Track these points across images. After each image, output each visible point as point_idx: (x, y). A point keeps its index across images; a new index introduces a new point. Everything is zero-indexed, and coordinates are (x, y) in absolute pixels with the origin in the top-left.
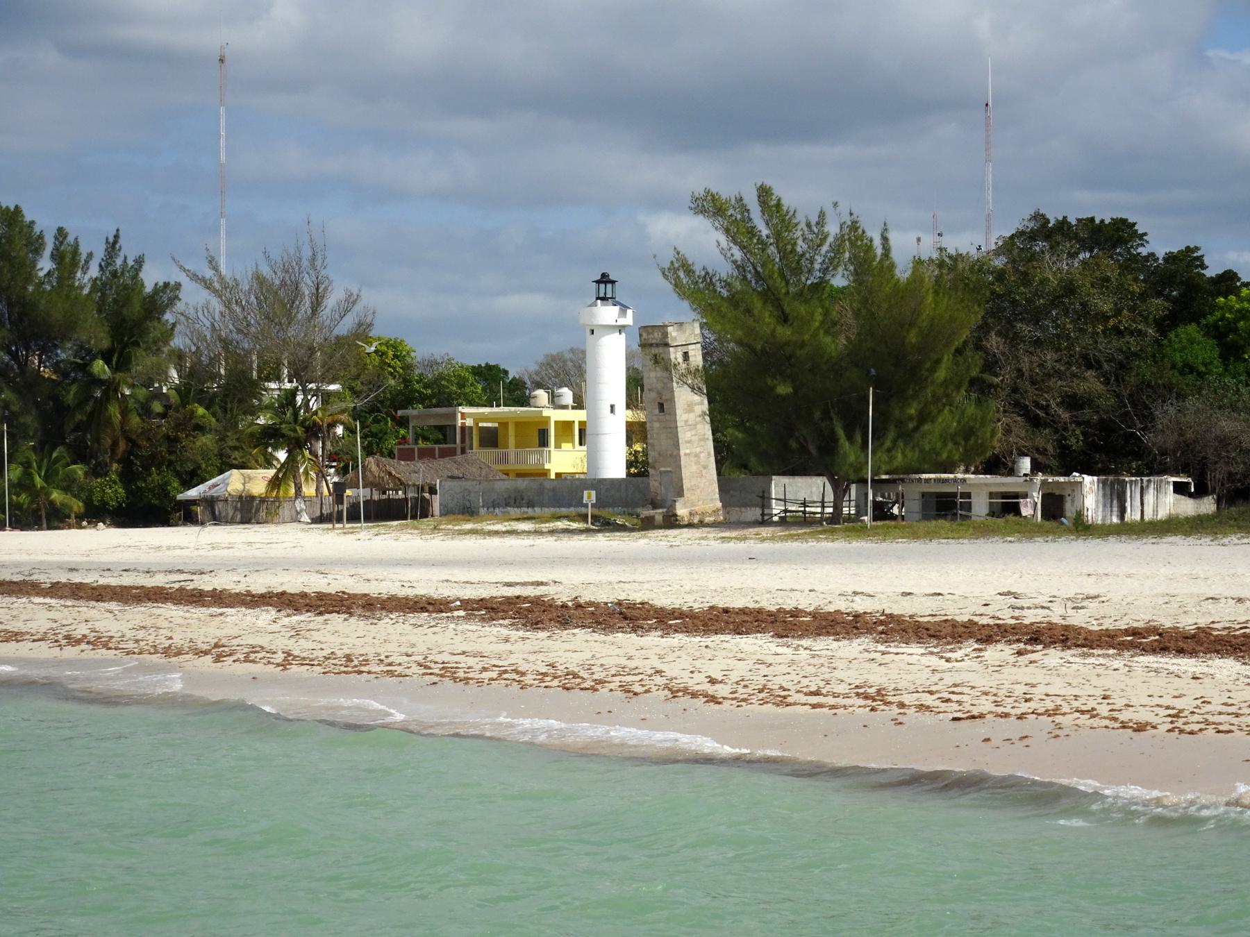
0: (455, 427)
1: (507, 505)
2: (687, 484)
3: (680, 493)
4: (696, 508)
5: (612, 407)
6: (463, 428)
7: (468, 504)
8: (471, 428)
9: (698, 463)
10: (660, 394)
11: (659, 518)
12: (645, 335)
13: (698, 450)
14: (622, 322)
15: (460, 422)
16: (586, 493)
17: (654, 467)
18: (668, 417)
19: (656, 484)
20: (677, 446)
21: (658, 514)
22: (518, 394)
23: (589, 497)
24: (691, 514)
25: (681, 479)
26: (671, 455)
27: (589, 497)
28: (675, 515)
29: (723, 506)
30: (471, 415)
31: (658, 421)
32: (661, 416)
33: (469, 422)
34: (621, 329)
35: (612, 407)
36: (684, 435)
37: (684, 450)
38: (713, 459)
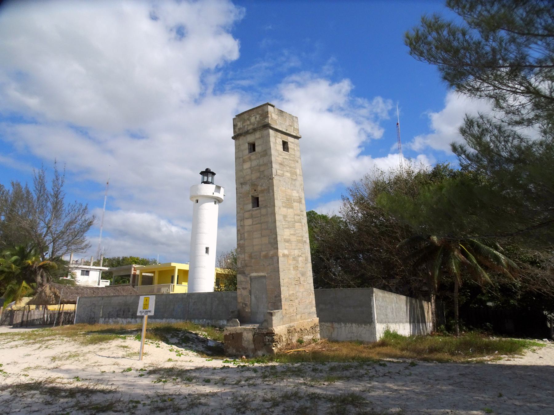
0: (129, 276)
1: (118, 316)
2: (285, 293)
3: (277, 304)
4: (295, 324)
5: (207, 249)
6: (135, 275)
7: (93, 316)
8: (138, 275)
9: (296, 268)
10: (254, 185)
11: (248, 336)
12: (240, 125)
13: (296, 252)
14: (216, 195)
15: (133, 272)
16: (142, 299)
17: (243, 273)
18: (263, 211)
19: (245, 293)
20: (274, 244)
21: (247, 331)
22: (289, 370)
23: (146, 306)
24: (289, 332)
25: (279, 286)
26: (266, 256)
27: (146, 306)
28: (271, 334)
29: (320, 321)
30: (138, 268)
31: (252, 217)
32: (256, 211)
33: (138, 272)
34: (217, 201)
35: (207, 249)
36: (284, 233)
37: (282, 251)
38: (310, 266)
